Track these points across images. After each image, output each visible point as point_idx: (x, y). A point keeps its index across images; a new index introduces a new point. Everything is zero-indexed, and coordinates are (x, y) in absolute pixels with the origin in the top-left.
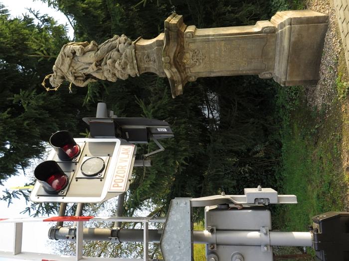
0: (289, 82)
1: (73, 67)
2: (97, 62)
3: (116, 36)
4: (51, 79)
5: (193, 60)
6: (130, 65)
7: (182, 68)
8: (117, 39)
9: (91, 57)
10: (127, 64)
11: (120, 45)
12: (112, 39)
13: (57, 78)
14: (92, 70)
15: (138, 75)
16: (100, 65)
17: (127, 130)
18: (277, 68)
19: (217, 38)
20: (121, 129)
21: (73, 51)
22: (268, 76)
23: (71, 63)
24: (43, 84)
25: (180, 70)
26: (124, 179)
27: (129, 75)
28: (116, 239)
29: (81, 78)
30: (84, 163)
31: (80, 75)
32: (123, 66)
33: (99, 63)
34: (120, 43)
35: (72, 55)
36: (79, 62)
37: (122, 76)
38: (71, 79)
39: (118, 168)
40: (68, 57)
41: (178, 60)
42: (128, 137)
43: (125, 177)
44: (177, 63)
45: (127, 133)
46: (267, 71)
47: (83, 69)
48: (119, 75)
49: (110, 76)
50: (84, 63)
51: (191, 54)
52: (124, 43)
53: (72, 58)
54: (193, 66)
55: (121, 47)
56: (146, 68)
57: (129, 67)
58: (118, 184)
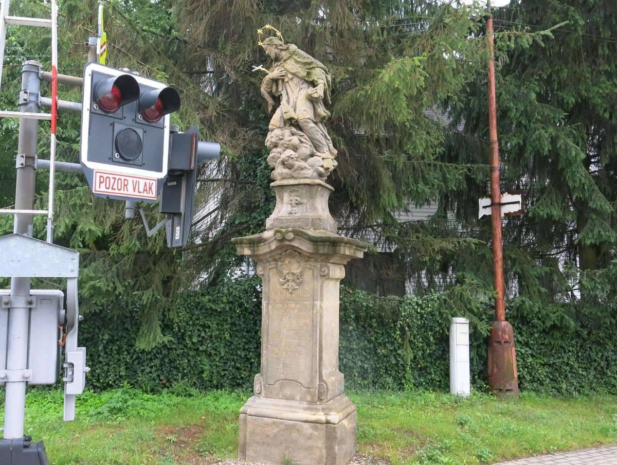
0: (245, 420)
1: (292, 79)
2: (297, 121)
3: (336, 152)
4: (276, 41)
5: (288, 274)
6: (287, 174)
7: (277, 257)
8: (331, 153)
9: (304, 112)
10: (290, 169)
11: (320, 159)
12: (331, 145)
13: (276, 51)
14: (284, 110)
15: (272, 184)
16: (292, 125)
17: (179, 186)
18: (268, 401)
19: (317, 313)
20: (181, 176)
21: (316, 83)
22: (257, 388)
23: (298, 77)
24: (268, 26)
25: (273, 254)
26: (110, 190)
27: (273, 169)
28: (22, 164)
29: (274, 90)
30: (135, 131)
31: (280, 89)
32: (286, 163)
33: (292, 123)
34: (323, 159)
35: (311, 80)
36: (299, 91)
37: (273, 158)
38: (274, 73)
39: (125, 180)
40: (308, 74)
41: (288, 252)
42: (169, 184)
43: (113, 191)
44: (286, 249)
45: (175, 183)
46: (265, 387)
47: (287, 94)
48: (274, 153)
49: (274, 140)
50: (297, 98)
51: (297, 271)
52: (322, 166)
53: (306, 79)
54: (280, 273)
55: (317, 161)
56: (282, 200)
57: (286, 171)
58: (102, 183)
